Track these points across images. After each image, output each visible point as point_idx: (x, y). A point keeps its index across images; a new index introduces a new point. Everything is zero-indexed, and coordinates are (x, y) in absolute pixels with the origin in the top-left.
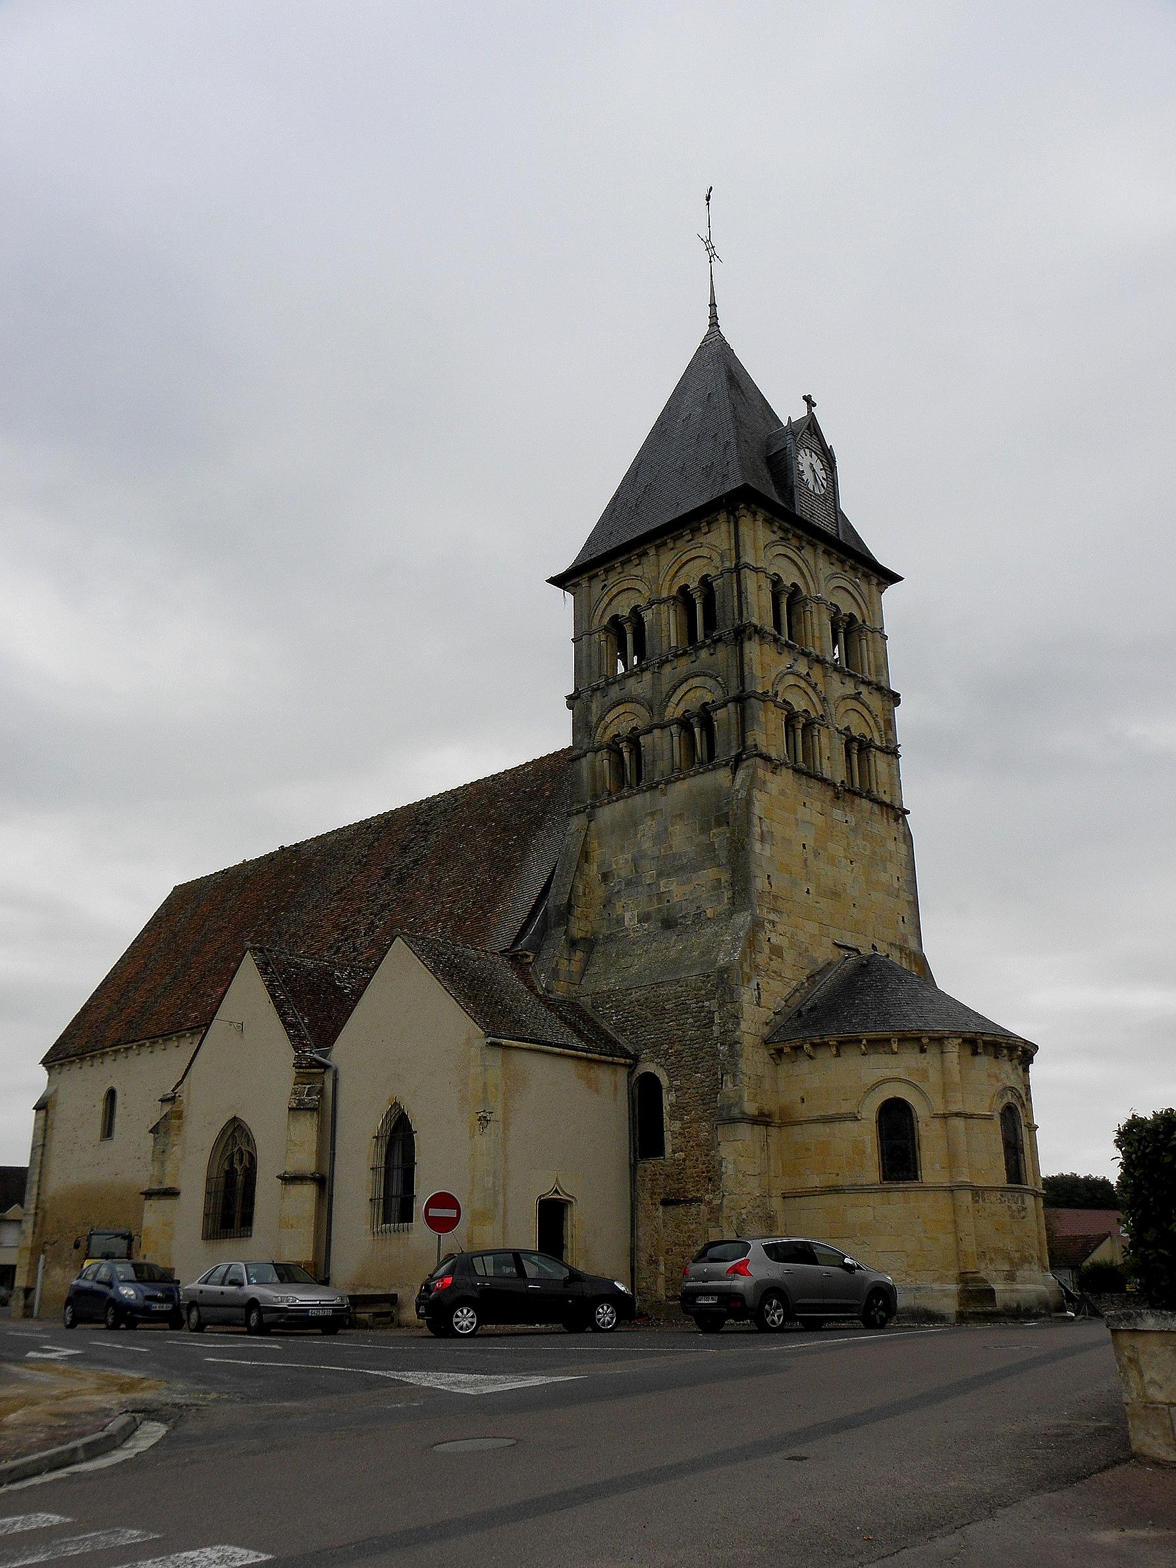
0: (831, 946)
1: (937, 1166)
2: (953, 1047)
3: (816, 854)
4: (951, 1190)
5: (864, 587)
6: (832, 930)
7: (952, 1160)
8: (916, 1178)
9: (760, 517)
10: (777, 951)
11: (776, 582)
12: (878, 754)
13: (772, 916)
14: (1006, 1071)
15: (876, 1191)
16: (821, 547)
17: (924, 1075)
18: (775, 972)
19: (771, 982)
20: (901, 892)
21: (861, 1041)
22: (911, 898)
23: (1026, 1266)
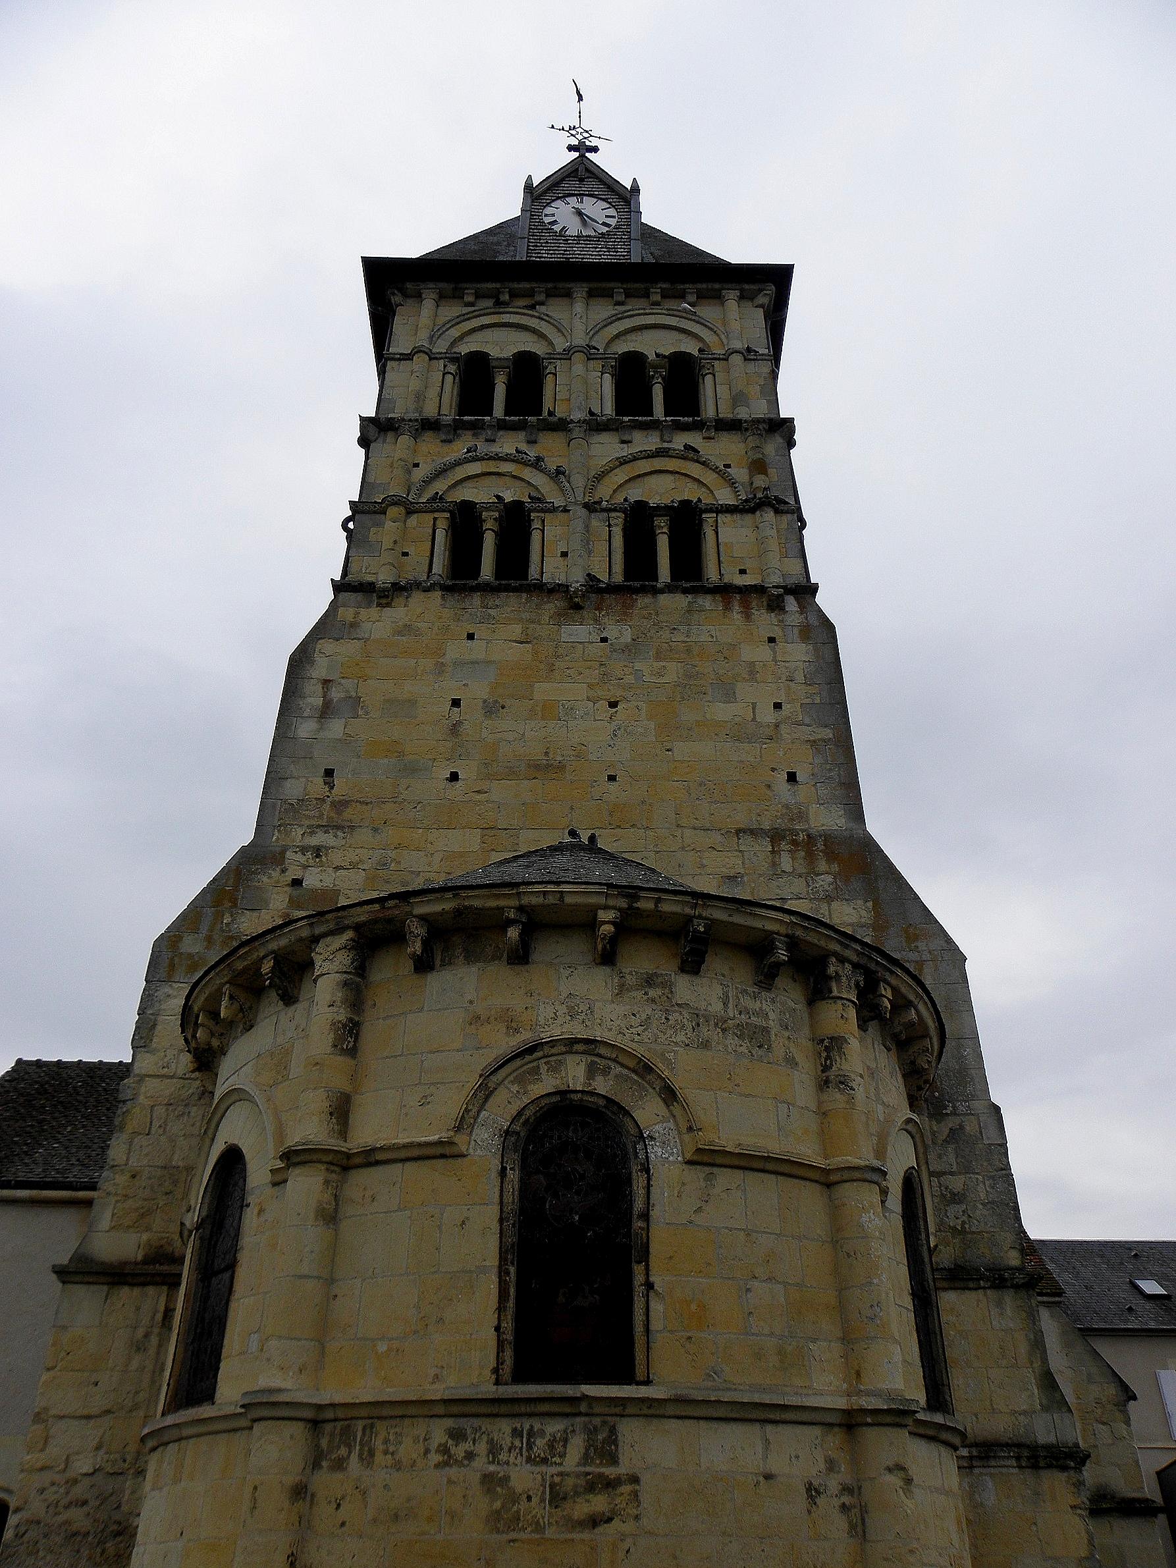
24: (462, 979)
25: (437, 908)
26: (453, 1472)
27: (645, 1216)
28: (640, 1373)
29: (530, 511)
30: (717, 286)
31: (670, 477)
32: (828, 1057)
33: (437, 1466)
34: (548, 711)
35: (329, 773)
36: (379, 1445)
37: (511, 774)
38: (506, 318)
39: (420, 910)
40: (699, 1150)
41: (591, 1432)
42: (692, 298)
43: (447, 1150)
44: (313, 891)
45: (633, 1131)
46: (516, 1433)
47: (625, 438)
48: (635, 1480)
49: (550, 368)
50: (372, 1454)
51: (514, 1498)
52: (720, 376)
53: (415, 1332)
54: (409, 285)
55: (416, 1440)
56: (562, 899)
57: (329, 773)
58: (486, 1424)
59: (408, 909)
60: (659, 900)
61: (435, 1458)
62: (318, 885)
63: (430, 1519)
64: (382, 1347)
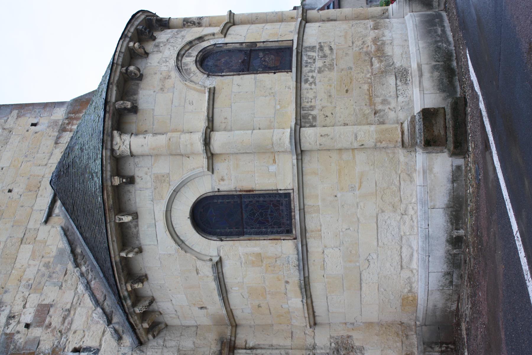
0: (48, 227)
1: (273, 168)
2: (123, 143)
4: (300, 153)
6: (31, 225)
7: (268, 151)
8: (287, 195)
10: (43, 311)
14: (162, 57)
15: (305, 245)
17: (161, 179)
18: (64, 319)
19: (74, 327)
20: (7, 126)
21: (122, 258)
22: (15, 112)
23: (388, 50)
24: (144, 96)
25: (114, 93)
26: (317, 81)
27: (241, 43)
28: (289, 43)
32: (190, 23)
33: (315, 85)
36: (308, 105)
39: (113, 99)
40: (222, 32)
41: (307, 51)
43: (212, 91)
45: (212, 47)
46: (306, 66)
48: (320, 43)
50: (311, 107)
51: (325, 66)
53: (274, 96)
55: (308, 93)
56: (122, 53)
58: (303, 74)
59: (112, 104)
60: (117, 64)
61: (313, 85)
63: (330, 86)
64: (278, 107)
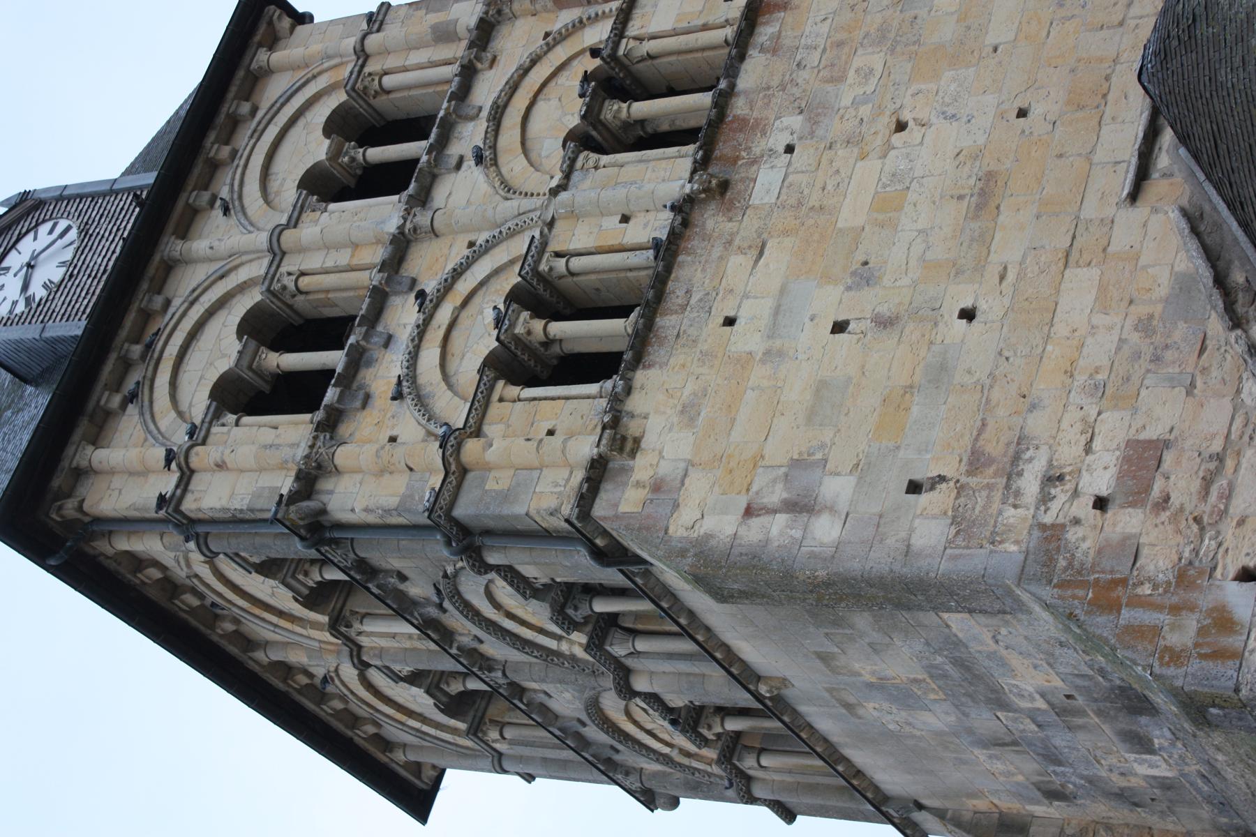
0: (1140, 211)
3: (865, 275)
5: (274, 89)
9: (262, 56)
10: (1144, 459)
11: (324, 186)
12: (634, 29)
13: (1030, 484)
16: (173, 247)
18: (1207, 482)
29: (535, 271)
30: (241, 73)
31: (541, 106)
34: (888, 206)
35: (914, 487)
37: (984, 240)
38: (173, 349)
42: (245, 108)
44: (1121, 477)
47: (454, 161)
49: (289, 282)
52: (390, 62)
54: (56, 483)
57: (914, 487)
62: (1113, 471)
